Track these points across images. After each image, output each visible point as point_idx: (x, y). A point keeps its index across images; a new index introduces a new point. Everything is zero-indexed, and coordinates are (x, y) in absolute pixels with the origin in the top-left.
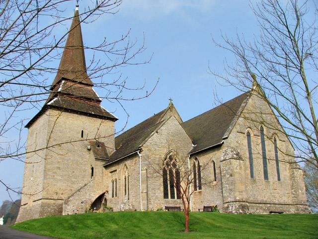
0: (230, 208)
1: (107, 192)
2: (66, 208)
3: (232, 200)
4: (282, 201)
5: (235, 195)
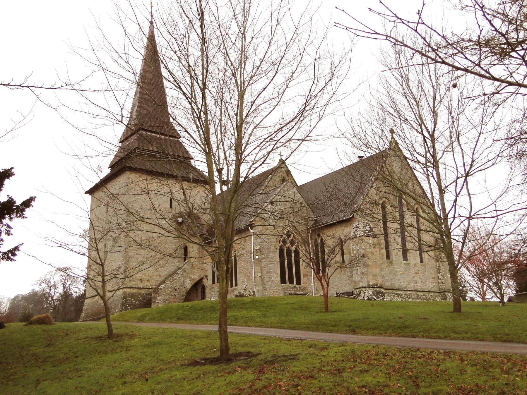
0: (363, 294)
1: (207, 276)
2: (155, 298)
3: (365, 285)
4: (425, 288)
5: (369, 279)
